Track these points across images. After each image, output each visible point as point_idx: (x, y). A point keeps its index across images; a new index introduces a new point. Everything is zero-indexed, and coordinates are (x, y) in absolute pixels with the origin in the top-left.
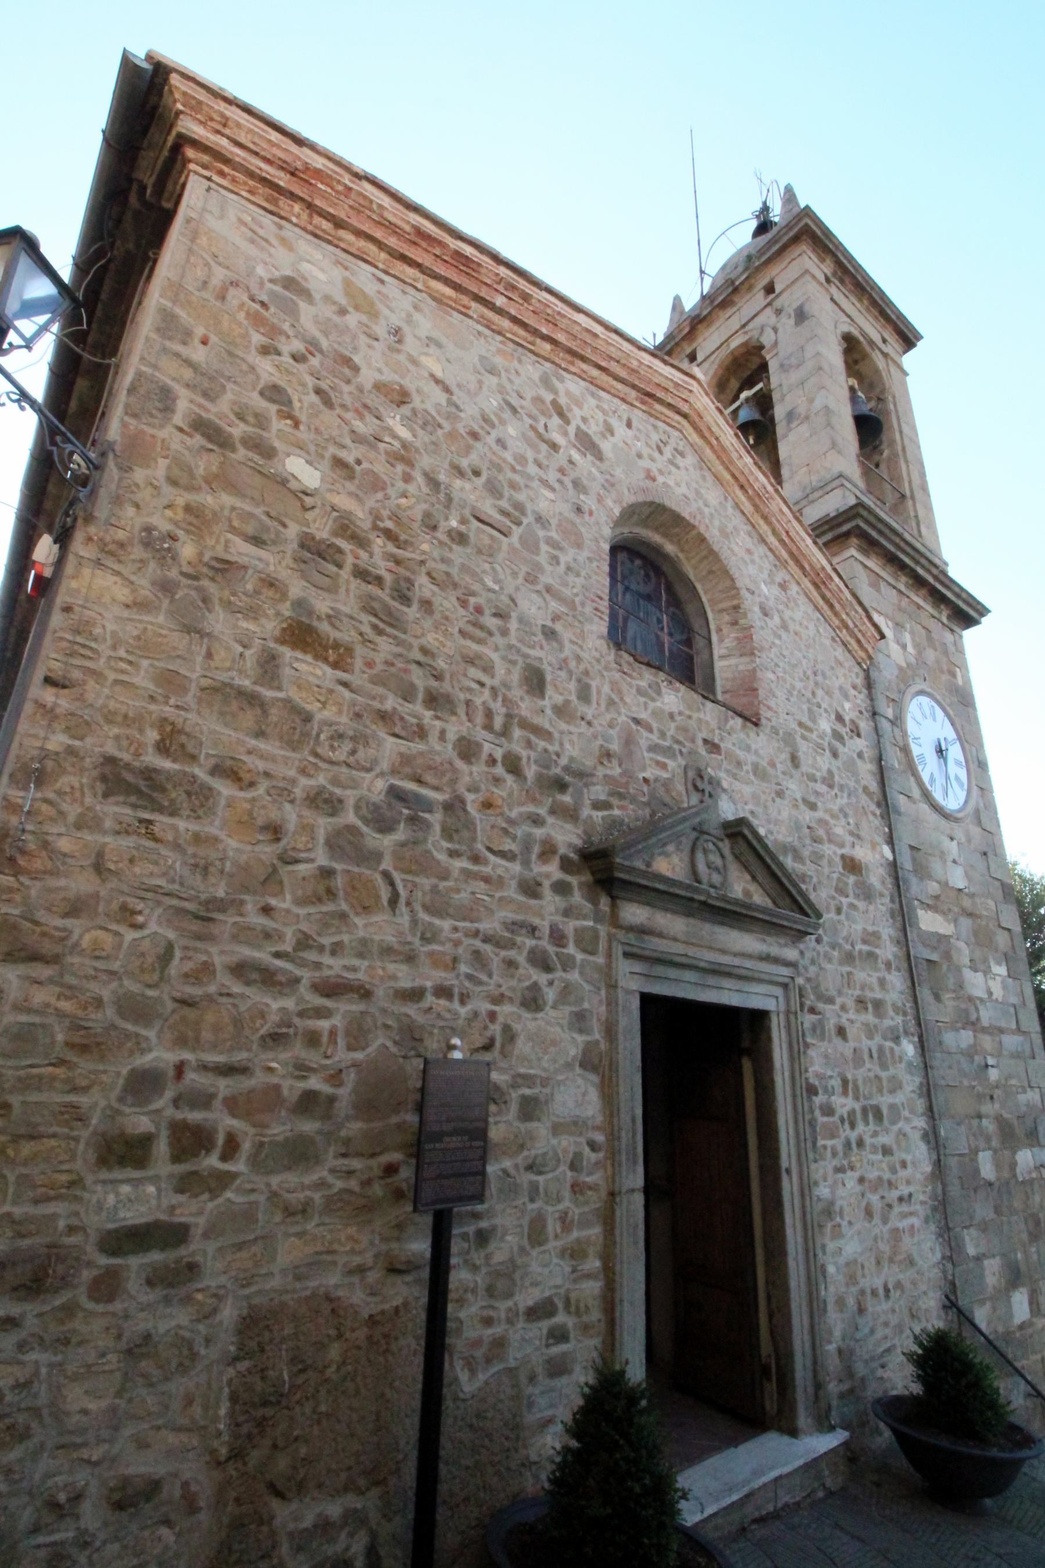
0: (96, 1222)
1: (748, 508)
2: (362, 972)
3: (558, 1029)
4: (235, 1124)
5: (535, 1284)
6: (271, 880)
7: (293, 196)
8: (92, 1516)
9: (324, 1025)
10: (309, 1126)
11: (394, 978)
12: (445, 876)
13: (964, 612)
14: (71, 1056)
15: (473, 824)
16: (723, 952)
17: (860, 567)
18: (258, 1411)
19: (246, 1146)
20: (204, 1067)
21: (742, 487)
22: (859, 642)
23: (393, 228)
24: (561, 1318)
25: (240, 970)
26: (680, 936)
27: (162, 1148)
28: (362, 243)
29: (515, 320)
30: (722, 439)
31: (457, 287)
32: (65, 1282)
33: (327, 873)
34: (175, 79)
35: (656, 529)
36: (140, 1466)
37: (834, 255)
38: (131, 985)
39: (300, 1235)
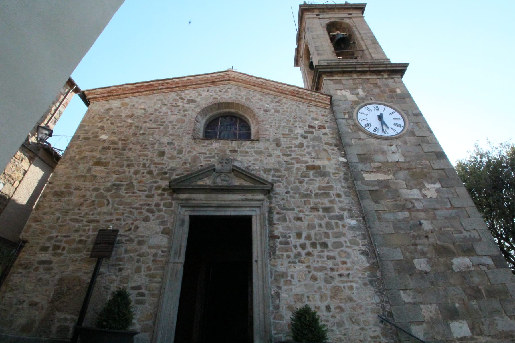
0: (38, 259)
1: (259, 89)
2: (98, 218)
3: (154, 225)
4: (65, 245)
5: (135, 281)
6: (82, 204)
7: (109, 96)
8: (25, 305)
9: (87, 228)
10: (80, 246)
11: (106, 218)
12: (124, 197)
13: (400, 70)
14: (40, 235)
15: (135, 186)
16: (225, 201)
17: (329, 81)
18: (59, 295)
19: (66, 249)
20: (62, 236)
21: (254, 86)
22: (320, 102)
23: (131, 89)
24: (143, 291)
25: (71, 220)
26: (202, 199)
27: (51, 249)
28: (126, 95)
29: (165, 88)
30: (243, 79)
31: (149, 91)
32: (30, 268)
33: (93, 201)
34: (86, 92)
35: (225, 108)
36: (36, 299)
37: (316, 8)
38: (51, 224)
39: (74, 265)
